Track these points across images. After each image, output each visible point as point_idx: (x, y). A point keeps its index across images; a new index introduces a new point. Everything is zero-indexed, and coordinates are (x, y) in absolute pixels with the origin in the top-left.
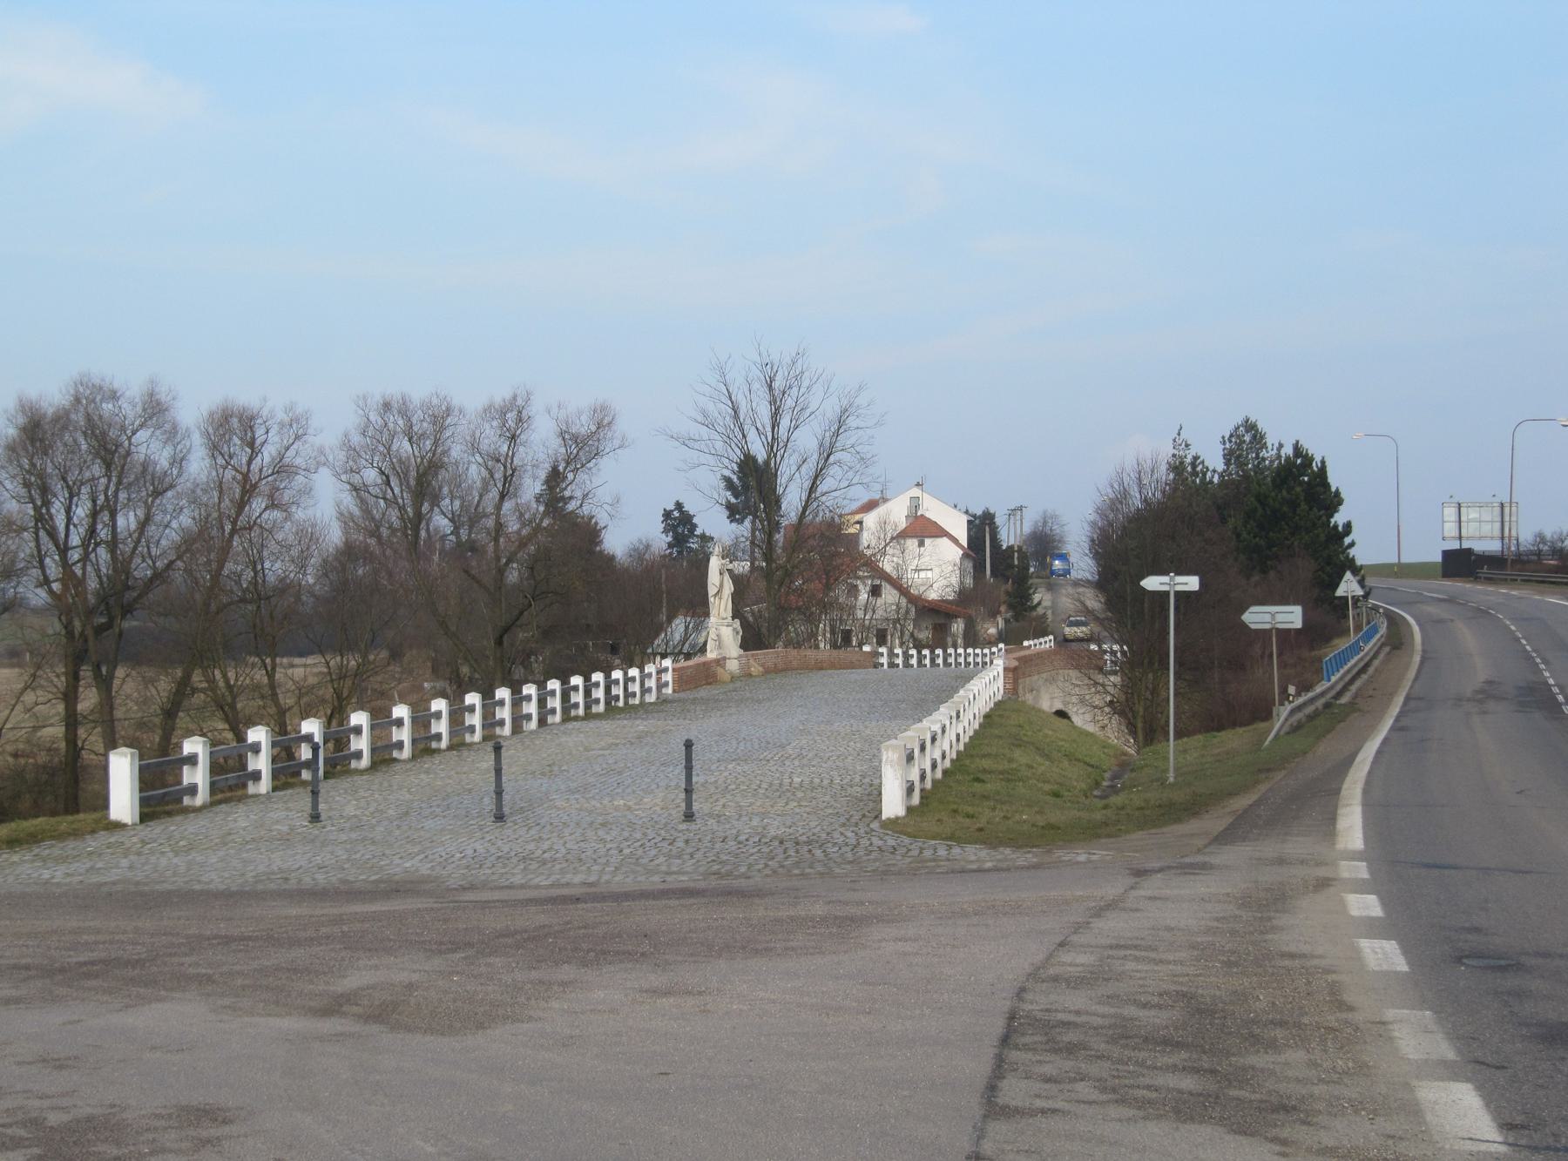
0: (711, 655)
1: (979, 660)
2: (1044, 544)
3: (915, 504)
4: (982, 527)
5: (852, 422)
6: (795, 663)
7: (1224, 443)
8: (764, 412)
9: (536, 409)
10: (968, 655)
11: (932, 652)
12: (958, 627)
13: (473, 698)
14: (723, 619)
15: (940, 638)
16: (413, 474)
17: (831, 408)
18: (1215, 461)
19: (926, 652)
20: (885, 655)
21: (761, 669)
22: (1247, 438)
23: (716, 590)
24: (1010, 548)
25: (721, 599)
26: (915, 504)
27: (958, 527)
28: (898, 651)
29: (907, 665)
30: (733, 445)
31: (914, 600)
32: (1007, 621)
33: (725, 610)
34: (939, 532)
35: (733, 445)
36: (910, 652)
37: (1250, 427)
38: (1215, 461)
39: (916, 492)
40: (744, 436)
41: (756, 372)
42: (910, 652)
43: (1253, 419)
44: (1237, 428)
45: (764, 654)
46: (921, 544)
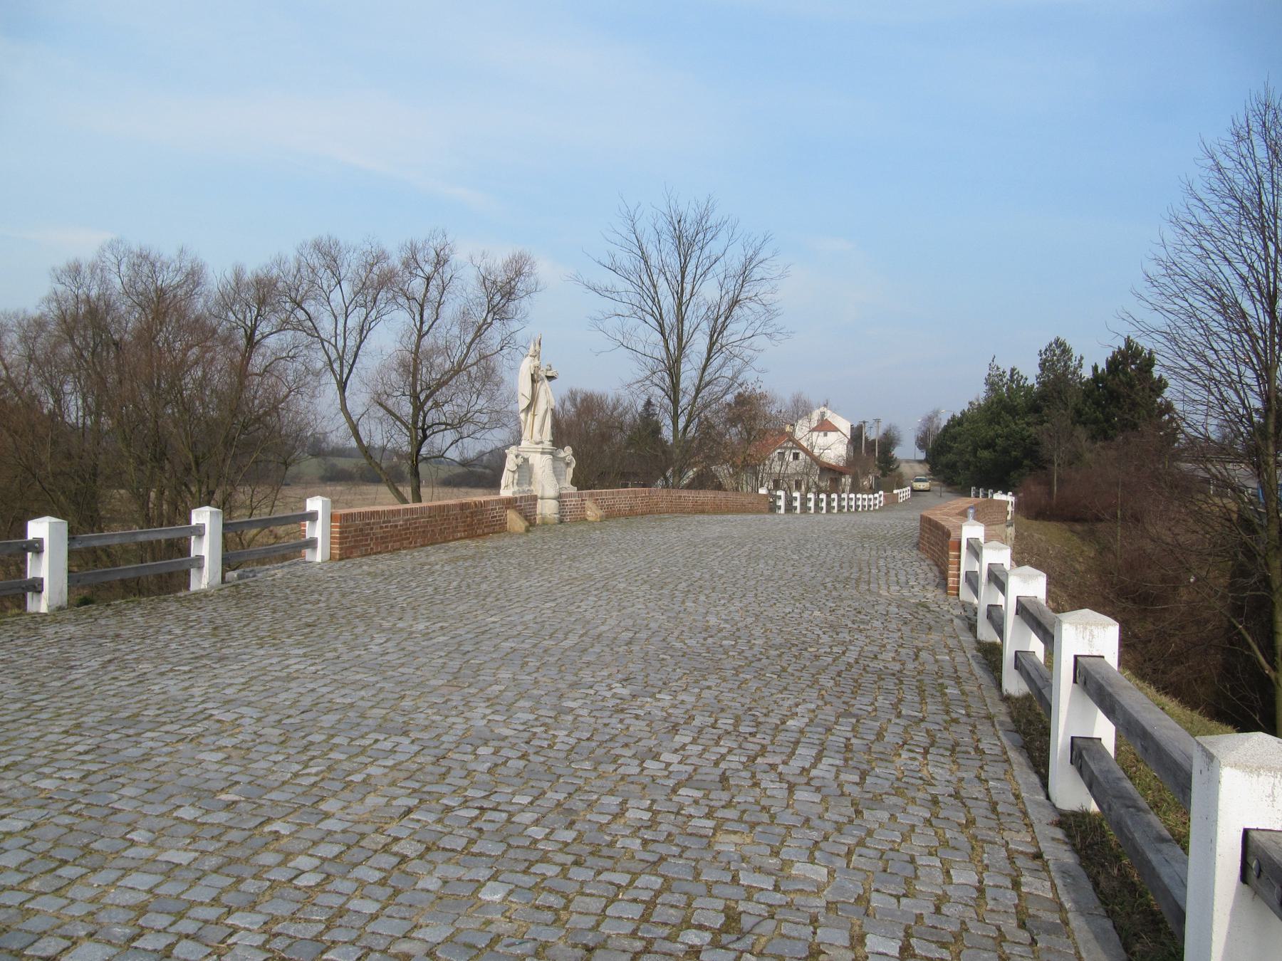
0: (507, 490)
1: (866, 503)
2: (888, 442)
3: (823, 414)
4: (856, 435)
5: (757, 273)
6: (663, 505)
7: (1041, 355)
8: (674, 262)
9: (459, 257)
10: (857, 499)
11: (829, 496)
12: (847, 480)
13: (823, 496)
14: (537, 443)
15: (835, 487)
16: (579, 400)
17: (734, 260)
18: (1031, 374)
19: (823, 496)
20: (783, 497)
21: (600, 513)
22: (1057, 352)
23: (527, 402)
24: (874, 441)
25: (534, 415)
26: (823, 414)
27: (845, 426)
28: (796, 494)
29: (805, 508)
30: (645, 297)
31: (816, 460)
32: (876, 478)
33: (541, 430)
34: (836, 429)
35: (645, 297)
36: (809, 496)
37: (1059, 343)
38: (1031, 374)
39: (822, 409)
40: (655, 286)
41: (662, 224)
42: (809, 496)
43: (1062, 339)
44: (1051, 345)
45: (613, 493)
46: (826, 435)
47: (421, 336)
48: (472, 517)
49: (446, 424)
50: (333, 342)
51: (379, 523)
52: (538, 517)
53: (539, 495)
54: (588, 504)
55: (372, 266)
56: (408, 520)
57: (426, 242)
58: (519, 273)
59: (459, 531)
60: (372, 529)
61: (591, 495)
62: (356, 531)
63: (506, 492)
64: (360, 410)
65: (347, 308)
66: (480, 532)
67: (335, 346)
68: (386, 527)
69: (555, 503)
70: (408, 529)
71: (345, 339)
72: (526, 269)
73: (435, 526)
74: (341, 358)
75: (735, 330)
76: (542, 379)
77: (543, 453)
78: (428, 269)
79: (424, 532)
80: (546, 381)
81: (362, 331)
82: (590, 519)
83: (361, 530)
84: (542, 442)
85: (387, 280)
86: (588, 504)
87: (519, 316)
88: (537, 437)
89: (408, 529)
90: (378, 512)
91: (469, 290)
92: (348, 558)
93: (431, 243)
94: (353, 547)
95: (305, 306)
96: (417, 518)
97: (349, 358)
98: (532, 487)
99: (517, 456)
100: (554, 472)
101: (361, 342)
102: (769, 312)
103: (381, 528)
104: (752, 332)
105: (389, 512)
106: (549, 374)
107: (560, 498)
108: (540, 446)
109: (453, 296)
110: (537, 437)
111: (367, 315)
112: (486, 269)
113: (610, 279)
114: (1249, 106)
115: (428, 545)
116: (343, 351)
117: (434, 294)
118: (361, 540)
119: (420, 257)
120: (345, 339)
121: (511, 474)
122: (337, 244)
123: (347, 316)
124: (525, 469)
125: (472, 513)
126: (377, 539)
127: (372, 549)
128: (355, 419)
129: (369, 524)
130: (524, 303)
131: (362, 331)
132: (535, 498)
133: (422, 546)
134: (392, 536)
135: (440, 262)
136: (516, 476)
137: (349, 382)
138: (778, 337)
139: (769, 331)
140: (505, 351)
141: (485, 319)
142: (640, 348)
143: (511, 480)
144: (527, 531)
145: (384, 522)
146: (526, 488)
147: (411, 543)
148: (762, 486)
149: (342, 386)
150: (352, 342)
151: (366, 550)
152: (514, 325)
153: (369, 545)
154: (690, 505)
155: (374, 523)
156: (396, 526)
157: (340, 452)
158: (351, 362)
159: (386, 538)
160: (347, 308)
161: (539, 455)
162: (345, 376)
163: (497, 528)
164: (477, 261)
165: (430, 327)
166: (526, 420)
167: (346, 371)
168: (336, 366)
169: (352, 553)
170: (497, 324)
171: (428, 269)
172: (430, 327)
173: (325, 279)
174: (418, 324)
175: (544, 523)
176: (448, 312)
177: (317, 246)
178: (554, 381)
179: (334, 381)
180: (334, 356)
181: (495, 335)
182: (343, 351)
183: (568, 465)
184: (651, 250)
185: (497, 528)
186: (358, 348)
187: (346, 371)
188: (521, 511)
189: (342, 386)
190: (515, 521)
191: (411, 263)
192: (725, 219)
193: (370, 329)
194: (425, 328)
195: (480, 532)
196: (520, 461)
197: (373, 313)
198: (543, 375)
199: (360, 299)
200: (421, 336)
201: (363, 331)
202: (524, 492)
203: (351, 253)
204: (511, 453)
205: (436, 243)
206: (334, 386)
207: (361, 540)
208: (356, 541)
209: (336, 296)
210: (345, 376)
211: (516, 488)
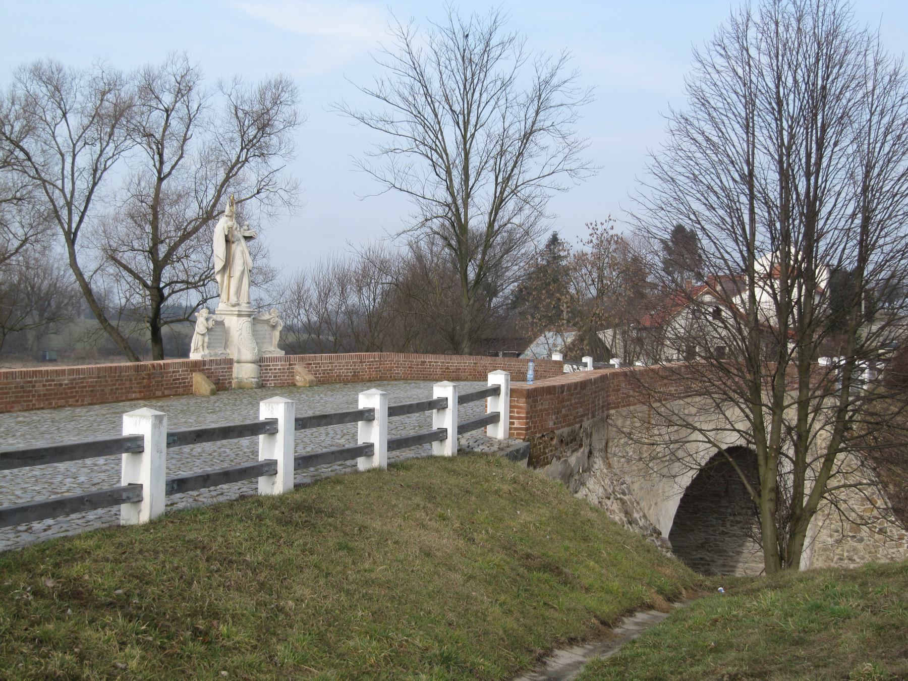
5: (556, 97)
6: (400, 371)
14: (234, 306)
17: (524, 86)
25: (230, 277)
47: (160, 180)
48: (149, 378)
49: (187, 283)
50: (60, 186)
51: (42, 381)
52: (234, 381)
53: (235, 358)
54: (299, 368)
55: (104, 94)
56: (75, 379)
57: (164, 68)
58: (276, 101)
59: (135, 392)
60: (34, 386)
61: (303, 359)
62: (16, 387)
63: (194, 356)
64: (93, 266)
65: (74, 145)
66: (158, 393)
67: (62, 190)
68: (50, 385)
69: (252, 367)
70: (75, 388)
71: (73, 183)
72: (285, 96)
73: (105, 386)
74: (69, 204)
75: (531, 168)
76: (239, 240)
77: (239, 315)
78: (167, 99)
79: (92, 391)
80: (243, 241)
81: (95, 171)
82: (299, 384)
83: (22, 387)
84: (238, 304)
85: (121, 112)
86: (299, 368)
87: (283, 152)
88: (233, 299)
89: (75, 388)
90: (40, 372)
91: (218, 122)
92: (8, 412)
93: (169, 69)
94: (13, 402)
95: (24, 144)
96: (84, 378)
97: (79, 203)
98: (228, 351)
99: (207, 320)
100: (253, 335)
101: (95, 184)
102: (572, 148)
103: (44, 386)
104: (553, 168)
105: (52, 371)
106: (247, 234)
107: (260, 362)
108: (236, 308)
109: (201, 130)
110: (233, 299)
111: (102, 151)
112: (237, 98)
113: (379, 108)
114: (764, 10)
115: (96, 404)
116: (72, 196)
117: (176, 125)
118: (22, 397)
119: (156, 85)
120: (73, 183)
121: (200, 337)
122: (59, 70)
123: (74, 156)
124: (218, 330)
125: (149, 375)
126: (39, 396)
127: (34, 405)
128: (86, 276)
129: (30, 382)
130: (291, 134)
131: (95, 171)
132: (230, 362)
133: (90, 404)
134: (56, 394)
135: (183, 90)
136: (206, 339)
137: (79, 233)
138: (583, 173)
139: (574, 166)
140: (263, 195)
141: (239, 157)
142: (417, 189)
143: (200, 343)
144: (213, 393)
145: (47, 381)
146: (220, 351)
147: (77, 401)
148: (638, 359)
149: (71, 238)
150: (82, 184)
151: (28, 406)
152: (275, 162)
153: (31, 401)
154: (439, 371)
155: (36, 382)
156: (61, 385)
157: (762, 325)
158: (82, 209)
159: (49, 395)
160: (74, 145)
161: (235, 318)
162: (74, 226)
163: (181, 390)
164: (228, 88)
165: (173, 168)
166: (223, 282)
167: (76, 219)
168: (64, 213)
169: (12, 407)
170: (253, 162)
171: (167, 99)
172: (173, 168)
173: (51, 113)
174: (157, 164)
175: (241, 387)
176: (194, 147)
177: (37, 73)
178: (252, 242)
179: (61, 231)
180: (61, 202)
181: (250, 174)
182: (72, 196)
183: (274, 327)
184: (431, 72)
185: (181, 390)
186: (91, 192)
187: (76, 219)
188: (209, 375)
189: (71, 238)
190: (202, 384)
191: (148, 90)
192: (513, 35)
193: (105, 169)
194: (166, 169)
195: (158, 393)
196: (211, 323)
197: (110, 150)
198: (240, 235)
199: (91, 133)
200: (160, 180)
201: (97, 172)
202: (216, 355)
203: (77, 80)
204: (201, 316)
205: (178, 68)
206: (62, 238)
207: (22, 397)
208: (16, 397)
209: (61, 131)
210: (74, 226)
211: (207, 351)
